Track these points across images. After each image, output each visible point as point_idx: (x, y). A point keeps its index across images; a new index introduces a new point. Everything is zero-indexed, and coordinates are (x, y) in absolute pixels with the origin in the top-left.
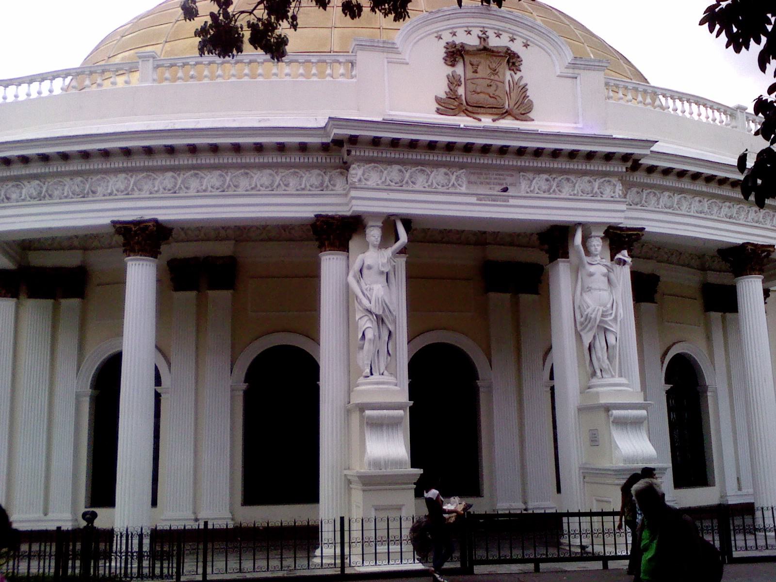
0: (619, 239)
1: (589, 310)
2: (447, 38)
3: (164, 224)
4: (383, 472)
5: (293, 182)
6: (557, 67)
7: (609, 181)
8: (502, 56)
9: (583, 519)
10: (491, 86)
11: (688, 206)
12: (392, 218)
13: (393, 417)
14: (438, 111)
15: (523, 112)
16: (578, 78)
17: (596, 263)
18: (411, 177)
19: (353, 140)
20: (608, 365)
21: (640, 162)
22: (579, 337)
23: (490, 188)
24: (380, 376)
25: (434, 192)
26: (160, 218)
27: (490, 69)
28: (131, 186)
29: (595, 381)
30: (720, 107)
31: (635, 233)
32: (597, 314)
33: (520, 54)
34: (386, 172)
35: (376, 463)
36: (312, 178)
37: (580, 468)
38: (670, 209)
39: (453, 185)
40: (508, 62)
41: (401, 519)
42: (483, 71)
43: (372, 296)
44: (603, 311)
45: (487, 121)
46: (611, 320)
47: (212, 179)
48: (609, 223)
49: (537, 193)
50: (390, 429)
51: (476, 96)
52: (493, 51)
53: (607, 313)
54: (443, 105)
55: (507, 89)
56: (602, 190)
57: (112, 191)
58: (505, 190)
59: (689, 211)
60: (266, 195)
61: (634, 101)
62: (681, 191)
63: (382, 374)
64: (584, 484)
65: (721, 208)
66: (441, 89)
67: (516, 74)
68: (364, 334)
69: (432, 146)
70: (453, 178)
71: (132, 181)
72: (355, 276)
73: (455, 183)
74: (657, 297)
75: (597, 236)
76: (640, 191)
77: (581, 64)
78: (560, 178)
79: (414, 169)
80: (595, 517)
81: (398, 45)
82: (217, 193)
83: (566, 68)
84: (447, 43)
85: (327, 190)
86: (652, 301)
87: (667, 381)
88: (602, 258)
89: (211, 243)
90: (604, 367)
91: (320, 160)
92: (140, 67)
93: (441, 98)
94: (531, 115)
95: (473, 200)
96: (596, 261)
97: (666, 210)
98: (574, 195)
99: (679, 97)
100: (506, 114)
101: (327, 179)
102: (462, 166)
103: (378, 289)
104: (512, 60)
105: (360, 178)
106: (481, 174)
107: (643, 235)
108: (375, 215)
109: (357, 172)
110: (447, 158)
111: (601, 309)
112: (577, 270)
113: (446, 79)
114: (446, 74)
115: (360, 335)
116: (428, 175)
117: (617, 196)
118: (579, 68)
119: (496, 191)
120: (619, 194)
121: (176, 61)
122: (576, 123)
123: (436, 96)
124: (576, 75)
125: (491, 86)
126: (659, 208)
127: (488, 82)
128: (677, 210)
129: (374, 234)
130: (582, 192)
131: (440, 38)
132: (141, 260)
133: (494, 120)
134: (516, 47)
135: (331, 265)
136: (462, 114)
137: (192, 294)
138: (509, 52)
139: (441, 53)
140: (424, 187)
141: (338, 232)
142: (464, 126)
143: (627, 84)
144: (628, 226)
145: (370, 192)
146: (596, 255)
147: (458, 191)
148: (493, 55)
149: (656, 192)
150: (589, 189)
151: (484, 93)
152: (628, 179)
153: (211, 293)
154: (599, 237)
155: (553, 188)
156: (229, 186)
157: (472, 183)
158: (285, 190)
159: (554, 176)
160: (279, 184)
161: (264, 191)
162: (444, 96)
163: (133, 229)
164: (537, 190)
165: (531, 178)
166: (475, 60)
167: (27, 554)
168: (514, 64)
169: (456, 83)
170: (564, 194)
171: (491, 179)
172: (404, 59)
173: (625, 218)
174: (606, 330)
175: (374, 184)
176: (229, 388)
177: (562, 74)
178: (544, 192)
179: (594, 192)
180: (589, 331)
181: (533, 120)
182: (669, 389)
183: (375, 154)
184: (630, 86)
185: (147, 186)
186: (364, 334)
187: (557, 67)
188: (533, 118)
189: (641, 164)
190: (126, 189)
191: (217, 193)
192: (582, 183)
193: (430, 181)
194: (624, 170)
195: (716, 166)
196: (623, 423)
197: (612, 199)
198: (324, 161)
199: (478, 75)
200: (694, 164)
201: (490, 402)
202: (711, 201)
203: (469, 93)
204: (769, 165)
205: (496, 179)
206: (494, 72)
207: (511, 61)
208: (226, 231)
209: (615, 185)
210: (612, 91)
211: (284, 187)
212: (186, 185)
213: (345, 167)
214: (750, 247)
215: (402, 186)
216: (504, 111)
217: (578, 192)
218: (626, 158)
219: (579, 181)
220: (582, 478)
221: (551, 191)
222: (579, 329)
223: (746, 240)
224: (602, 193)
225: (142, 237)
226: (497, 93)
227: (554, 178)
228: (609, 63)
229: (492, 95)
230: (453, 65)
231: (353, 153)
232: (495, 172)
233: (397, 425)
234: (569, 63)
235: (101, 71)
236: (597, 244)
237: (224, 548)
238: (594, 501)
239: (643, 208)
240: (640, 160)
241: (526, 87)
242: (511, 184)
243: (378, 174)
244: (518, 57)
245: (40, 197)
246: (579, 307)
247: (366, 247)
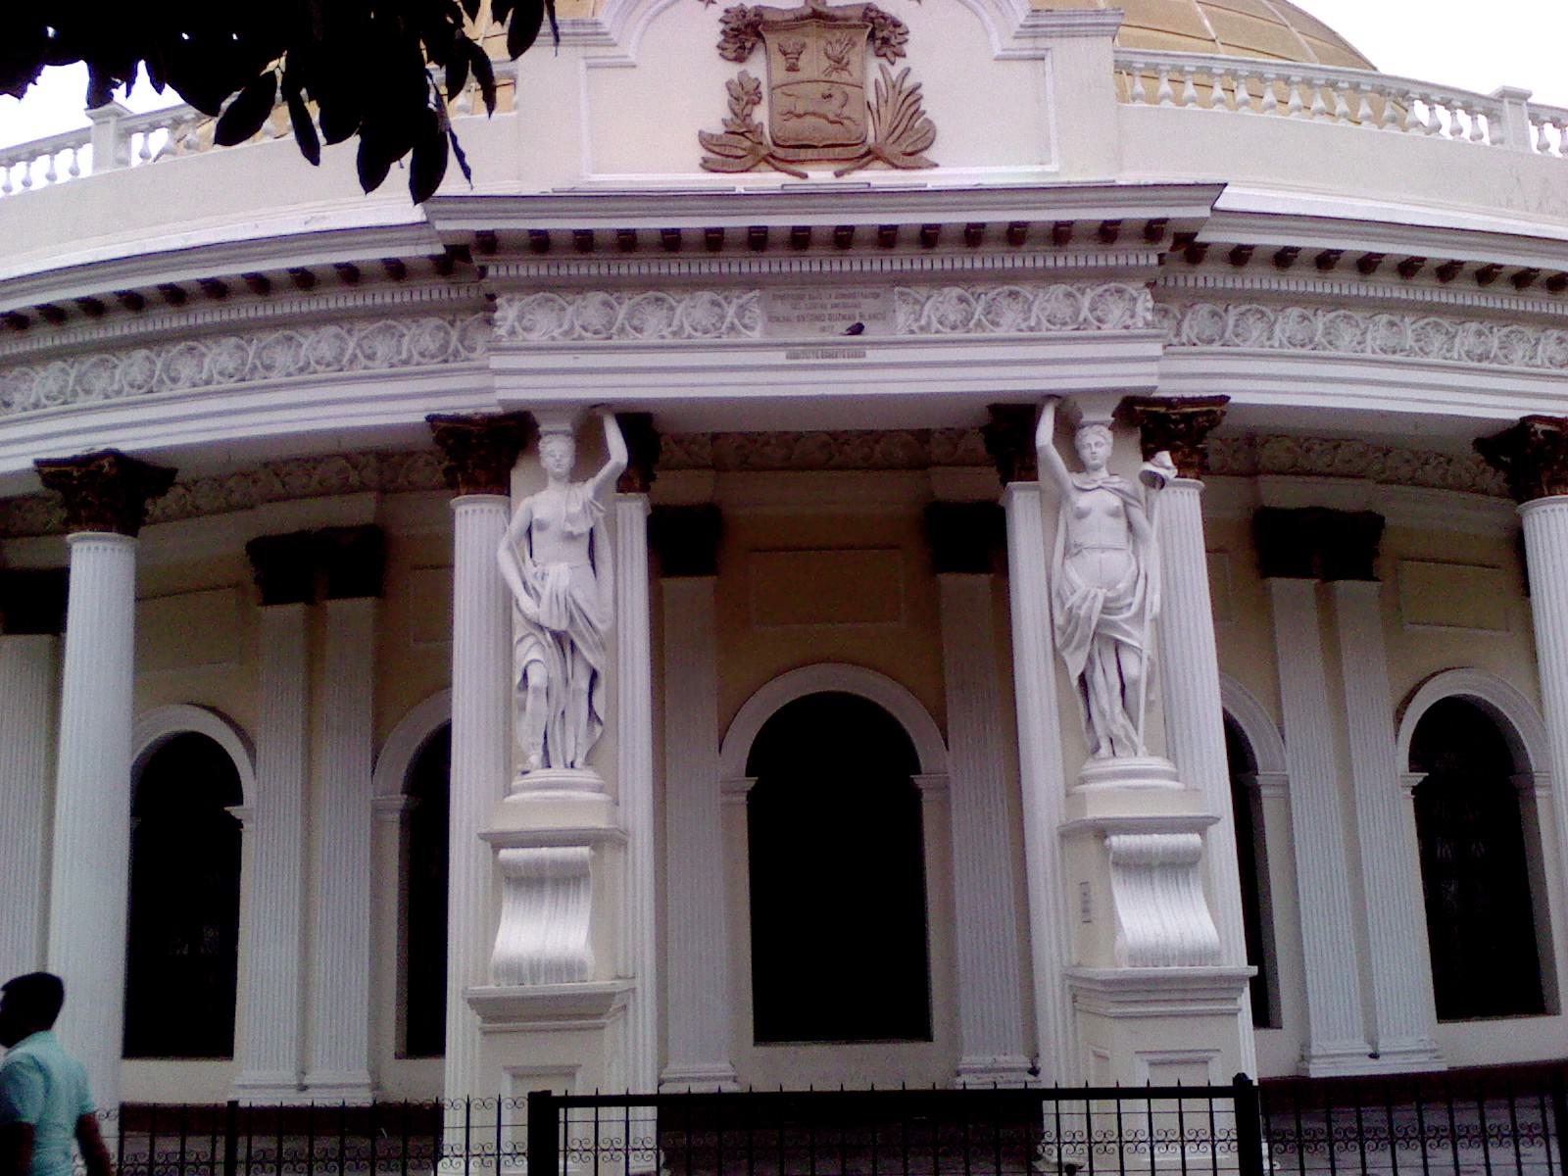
0: (1160, 425)
1: (1073, 600)
3: (146, 459)
4: (529, 988)
5: (383, 347)
6: (995, 36)
7: (1120, 291)
8: (855, 26)
9: (1158, 1104)
10: (830, 96)
11: (1359, 338)
13: (564, 865)
14: (707, 166)
15: (909, 150)
16: (1048, 60)
17: (1095, 486)
18: (630, 316)
19: (488, 242)
20: (1123, 727)
21: (1199, 239)
22: (1060, 664)
23: (823, 330)
24: (566, 770)
25: (686, 347)
26: (125, 447)
27: (829, 58)
28: (71, 384)
29: (1091, 767)
30: (1449, 96)
31: (1205, 409)
32: (1091, 609)
33: (902, 18)
34: (570, 310)
35: (511, 970)
36: (423, 336)
37: (1065, 976)
38: (1306, 348)
39: (732, 328)
40: (872, 37)
41: (468, 1106)
42: (814, 63)
43: (543, 587)
44: (1107, 600)
45: (821, 176)
46: (1126, 621)
47: (220, 356)
48: (1124, 390)
49: (937, 332)
50: (561, 895)
51: (794, 124)
52: (833, 18)
53: (1118, 605)
54: (717, 149)
55: (873, 100)
56: (1331, 337)
57: (39, 400)
58: (858, 329)
59: (1359, 348)
60: (327, 381)
61: (1280, 107)
62: (1337, 303)
63: (572, 766)
64: (1074, 1015)
65: (1454, 337)
66: (714, 115)
67: (893, 63)
69: (671, 241)
70: (731, 311)
71: (73, 373)
72: (510, 548)
73: (736, 321)
74: (1383, 565)
75: (1095, 423)
76: (1220, 309)
77: (1053, 26)
78: (992, 294)
79: (638, 298)
80: (576, 1110)
81: (607, 27)
82: (231, 384)
83: (1016, 38)
84: (727, 11)
85: (455, 361)
86: (1368, 576)
87: (1416, 761)
88: (1111, 475)
89: (336, 499)
90: (1115, 731)
91: (435, 296)
92: (93, 136)
93: (712, 136)
94: (930, 155)
95: (779, 357)
96: (1095, 481)
97: (1293, 351)
98: (1031, 329)
99: (1421, 95)
100: (870, 156)
101: (454, 335)
102: (750, 283)
103: (560, 573)
104: (883, 33)
105: (513, 327)
106: (801, 298)
107: (1224, 413)
108: (557, 407)
109: (507, 312)
110: (710, 267)
111: (1101, 594)
112: (1055, 505)
113: (725, 88)
114: (725, 81)
115: (518, 678)
116: (672, 309)
117: (1140, 325)
118: (1046, 36)
119: (837, 332)
120: (1144, 319)
121: (160, 117)
122: (1041, 164)
123: (700, 132)
124: (1039, 53)
125: (830, 96)
126: (1272, 346)
127: (824, 88)
128: (1324, 348)
130: (1049, 321)
132: (93, 539)
133: (838, 174)
135: (476, 527)
136: (763, 166)
137: (295, 610)
138: (873, 14)
139: (714, 33)
140: (663, 337)
141: (485, 451)
142: (745, 189)
143: (1179, 62)
144: (1187, 395)
145: (539, 357)
146: (1096, 468)
147: (742, 340)
148: (835, 27)
149: (1264, 309)
151: (814, 114)
152: (1181, 283)
153: (334, 606)
154: (1102, 424)
155: (976, 317)
156: (254, 368)
157: (778, 320)
158: (365, 368)
159: (980, 289)
160: (355, 356)
161: (324, 372)
162: (718, 129)
163: (75, 474)
164: (935, 325)
165: (923, 300)
166: (791, 41)
167: (1429, 1142)
168: (885, 41)
169: (745, 98)
170: (1005, 328)
171: (824, 307)
172: (626, 57)
173: (1163, 376)
174: (1118, 645)
175: (544, 338)
176: (369, 805)
177: (1006, 53)
178: (954, 328)
179: (1081, 318)
180: (1078, 647)
181: (936, 165)
182: (1420, 784)
183: (543, 272)
184: (1270, 73)
185: (100, 381)
186: (525, 676)
187: (995, 36)
188: (937, 162)
189: (1206, 245)
190: (61, 392)
191: (231, 384)
192: (1051, 300)
193: (676, 322)
194: (1154, 260)
195: (1421, 234)
196: (1141, 867)
197: (1124, 332)
198: (445, 295)
199: (798, 76)
200: (1359, 233)
201: (945, 828)
202: (1422, 323)
203: (778, 119)
204: (51, 31)
205: (835, 306)
206: (840, 63)
207: (879, 34)
208: (360, 472)
209: (1134, 300)
210: (1195, 84)
211: (364, 362)
212: (172, 375)
213: (489, 303)
214: (1539, 427)
215: (610, 338)
216: (863, 150)
217: (1039, 323)
218: (1153, 231)
219: (1041, 295)
220: (1068, 998)
221: (972, 324)
222: (1058, 645)
223: (1531, 409)
224: (1100, 320)
225: (110, 490)
226: (846, 112)
227: (979, 295)
228: (1122, 14)
229: (832, 117)
230: (740, 59)
231: (492, 272)
232: (834, 293)
233: (579, 881)
234: (1022, 26)
235: (27, 155)
236: (1098, 440)
237: (1386, 1139)
238: (1091, 1053)
239: (1226, 349)
240: (1196, 234)
241: (919, 91)
242: (874, 317)
243: (554, 315)
244: (897, 25)
246: (1059, 594)
247: (541, 482)
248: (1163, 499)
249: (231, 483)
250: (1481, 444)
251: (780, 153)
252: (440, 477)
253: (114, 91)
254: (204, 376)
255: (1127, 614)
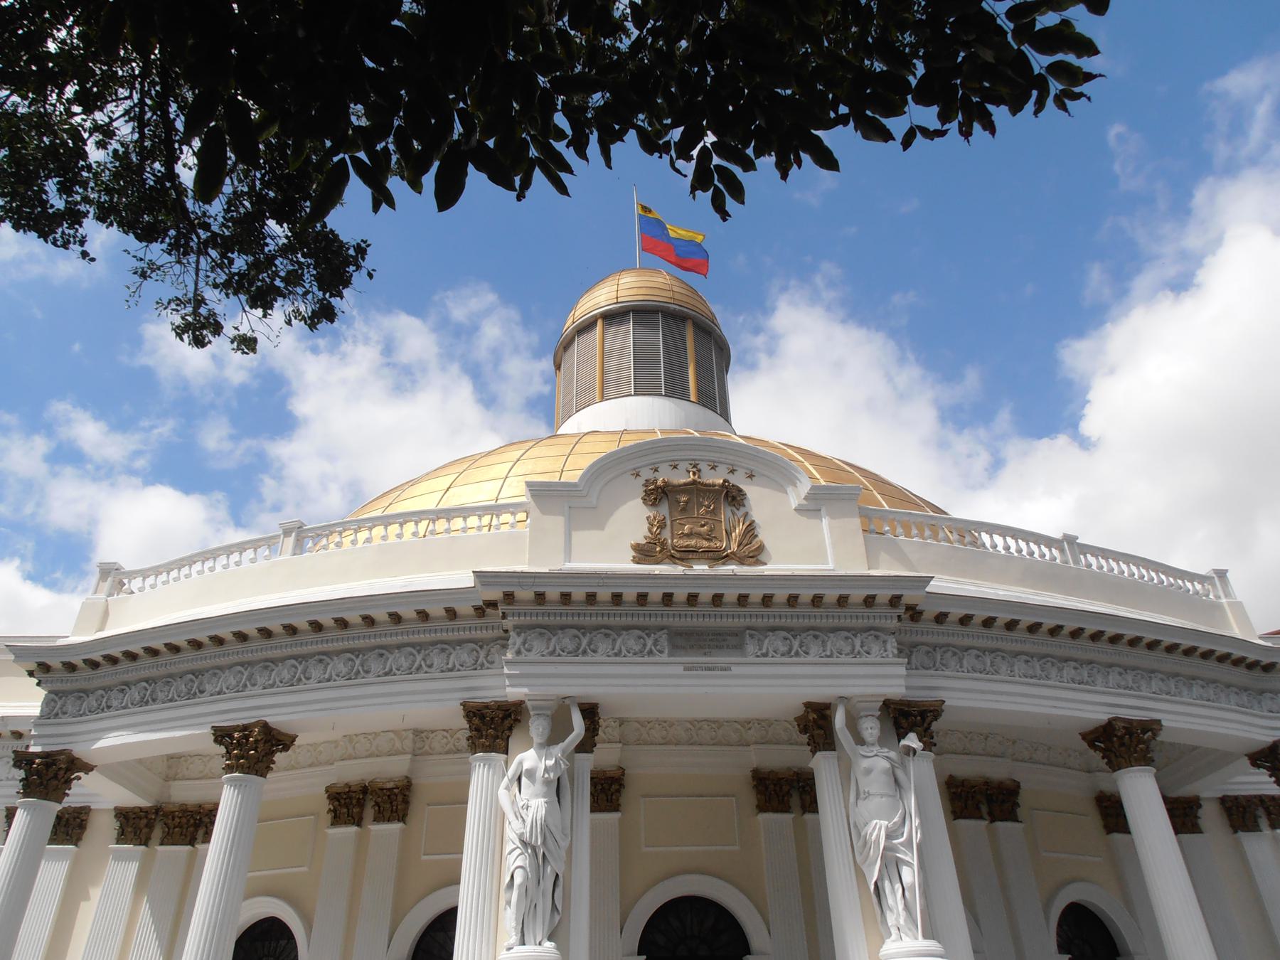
2: (647, 474)
12: (567, 701)
14: (636, 561)
45: (701, 568)
46: (901, 844)
68: (512, 877)
104: (733, 496)
116: (614, 640)
129: (537, 728)
131: (638, 475)
134: (738, 480)
150: (848, 649)
168: (734, 498)
178: (783, 655)
186: (512, 877)
245: (143, 702)
246: (856, 826)
248: (912, 764)
249: (321, 748)
250: (1084, 736)
251: (678, 555)
252: (464, 743)
253: (935, 109)
254: (327, 676)
255: (901, 840)
